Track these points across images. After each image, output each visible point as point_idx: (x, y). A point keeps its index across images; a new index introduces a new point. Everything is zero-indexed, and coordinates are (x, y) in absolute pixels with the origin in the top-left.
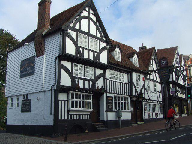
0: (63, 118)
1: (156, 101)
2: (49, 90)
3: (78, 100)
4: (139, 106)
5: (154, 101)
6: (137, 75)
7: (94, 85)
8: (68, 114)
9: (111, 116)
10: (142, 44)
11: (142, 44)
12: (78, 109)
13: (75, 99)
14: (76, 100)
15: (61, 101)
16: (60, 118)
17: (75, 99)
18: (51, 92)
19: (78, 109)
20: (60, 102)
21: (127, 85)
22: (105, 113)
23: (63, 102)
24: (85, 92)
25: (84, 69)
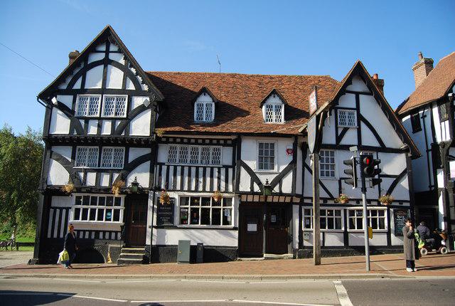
3: (90, 207)
6: (261, 145)
15: (55, 208)
16: (49, 236)
20: (52, 210)
21: (230, 171)
23: (58, 211)
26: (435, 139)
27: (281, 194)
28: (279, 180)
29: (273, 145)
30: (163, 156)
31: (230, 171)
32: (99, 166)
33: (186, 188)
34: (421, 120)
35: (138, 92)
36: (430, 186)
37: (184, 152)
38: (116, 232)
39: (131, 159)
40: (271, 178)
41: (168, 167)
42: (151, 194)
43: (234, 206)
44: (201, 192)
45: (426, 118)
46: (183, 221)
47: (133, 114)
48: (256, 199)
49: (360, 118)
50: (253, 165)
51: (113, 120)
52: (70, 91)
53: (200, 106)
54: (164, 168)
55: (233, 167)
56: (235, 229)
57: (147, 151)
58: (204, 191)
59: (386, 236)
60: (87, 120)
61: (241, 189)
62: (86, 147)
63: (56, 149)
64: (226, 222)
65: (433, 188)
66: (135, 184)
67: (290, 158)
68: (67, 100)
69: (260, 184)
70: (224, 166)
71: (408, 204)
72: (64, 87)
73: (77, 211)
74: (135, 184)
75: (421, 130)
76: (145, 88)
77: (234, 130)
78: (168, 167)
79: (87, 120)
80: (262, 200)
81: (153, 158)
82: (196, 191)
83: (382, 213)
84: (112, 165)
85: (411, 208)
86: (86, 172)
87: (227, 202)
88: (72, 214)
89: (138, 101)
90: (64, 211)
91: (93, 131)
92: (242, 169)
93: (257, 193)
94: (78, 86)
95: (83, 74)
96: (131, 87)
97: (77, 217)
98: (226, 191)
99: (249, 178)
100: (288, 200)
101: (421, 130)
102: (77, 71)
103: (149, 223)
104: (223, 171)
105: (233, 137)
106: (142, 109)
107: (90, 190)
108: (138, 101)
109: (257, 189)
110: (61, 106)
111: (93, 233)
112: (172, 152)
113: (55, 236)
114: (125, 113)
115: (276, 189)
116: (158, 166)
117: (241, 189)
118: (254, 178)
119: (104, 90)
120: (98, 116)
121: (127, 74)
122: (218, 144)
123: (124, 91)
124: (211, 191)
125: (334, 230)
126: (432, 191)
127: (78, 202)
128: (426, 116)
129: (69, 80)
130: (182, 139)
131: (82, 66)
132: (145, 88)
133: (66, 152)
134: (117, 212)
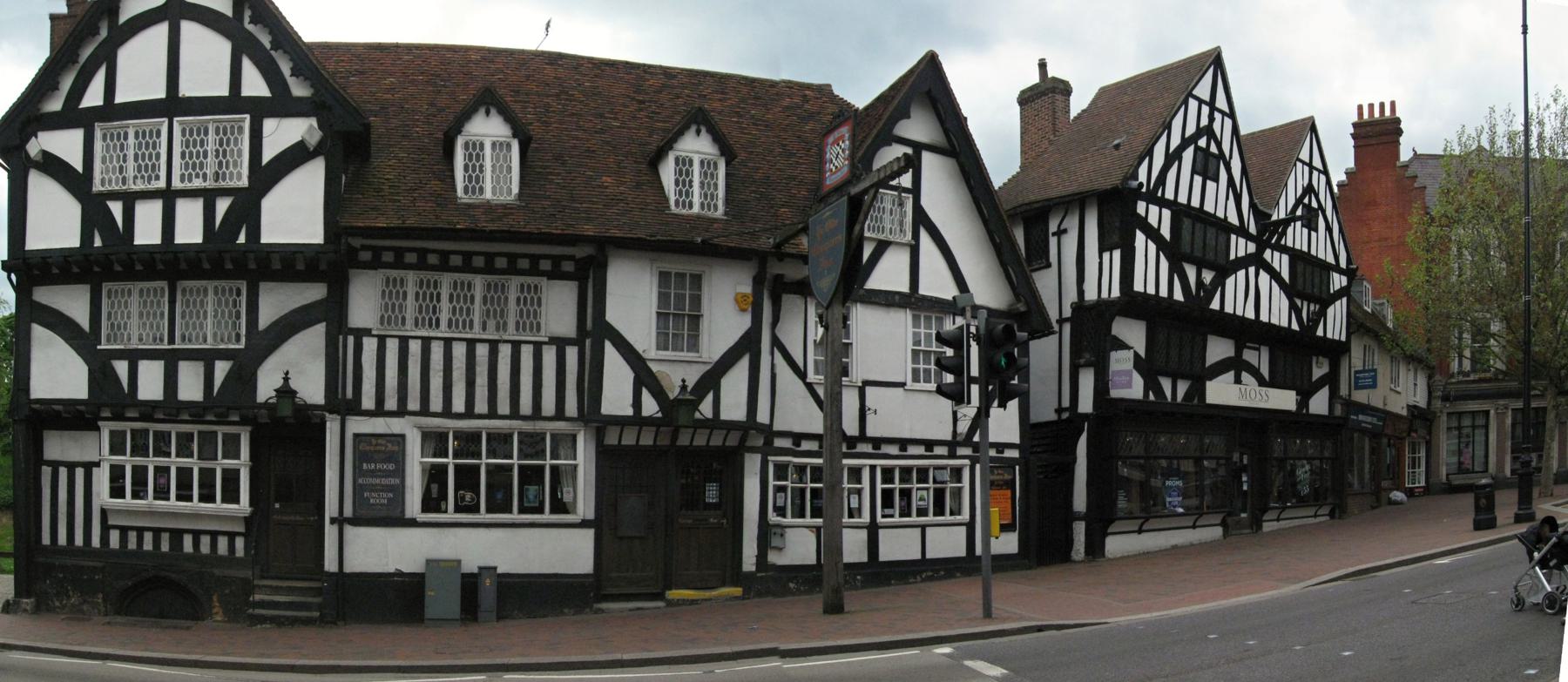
0: (79, 540)
1: (929, 444)
2: (1483, 426)
3: (151, 462)
4: (280, 505)
5: (903, 443)
6: (664, 278)
7: (244, 376)
8: (106, 528)
9: (800, 547)
10: (1043, 65)
11: (1043, 65)
12: (173, 503)
13: (195, 460)
14: (139, 460)
15: (55, 465)
16: (46, 540)
17: (127, 457)
18: (618, 433)
19: (149, 502)
20: (46, 471)
21: (572, 354)
22: (330, 532)
23: (63, 472)
24: (186, 417)
25: (172, 303)
26: (1081, 292)
27: (715, 423)
28: (711, 380)
29: (697, 280)
30: (364, 306)
31: (572, 354)
32: (172, 340)
33: (436, 404)
34: (1053, 241)
35: (281, 105)
36: (1059, 410)
37: (429, 298)
38: (231, 536)
39: (265, 318)
40: (693, 376)
41: (382, 340)
42: (332, 426)
43: (584, 457)
44: (481, 417)
45: (1065, 238)
46: (432, 502)
47: (267, 175)
48: (647, 440)
49: (918, 210)
50: (642, 333)
51: (209, 197)
52: (72, 117)
53: (475, 150)
54: (370, 345)
55: (578, 342)
56: (584, 524)
57: (314, 293)
58: (492, 414)
59: (963, 530)
60: (130, 200)
61: (608, 408)
62: (128, 285)
63: (46, 296)
64: (559, 507)
65: (1065, 415)
66: (286, 392)
67: (745, 322)
68: (66, 144)
69: (659, 393)
70: (553, 340)
71: (1015, 454)
72: (55, 105)
73: (117, 474)
74: (286, 392)
75: (1049, 265)
76: (299, 89)
77: (589, 230)
78: (382, 340)
79: (130, 200)
80: (664, 441)
81: (333, 312)
82: (469, 413)
83: (957, 473)
84: (209, 339)
85: (1023, 461)
86: (133, 357)
87: (565, 443)
88: (102, 479)
89: (282, 134)
90: (80, 473)
91: (147, 230)
92: (609, 348)
93: (650, 421)
94: (93, 97)
95: (107, 56)
96: (254, 85)
97: (117, 492)
98: (560, 414)
99: (629, 375)
100: (733, 441)
101: (1049, 265)
102: (86, 53)
103: (331, 509)
104: (549, 355)
105: (581, 252)
106: (295, 157)
107: (149, 411)
108: (282, 134)
109: (650, 407)
110: (53, 166)
111: (165, 537)
112: (394, 296)
113: (62, 539)
114: (245, 171)
115: (706, 408)
116: (351, 339)
117: (608, 408)
118: (644, 377)
119: (173, 105)
120: (162, 184)
121: (242, 47)
122: (534, 271)
123: (234, 102)
124: (515, 414)
125: (948, 518)
126: (1063, 421)
127: (117, 448)
128: (1065, 231)
129: (67, 83)
130: (423, 253)
131: (104, 33)
132: (299, 89)
133: (74, 303)
134: (231, 478)
